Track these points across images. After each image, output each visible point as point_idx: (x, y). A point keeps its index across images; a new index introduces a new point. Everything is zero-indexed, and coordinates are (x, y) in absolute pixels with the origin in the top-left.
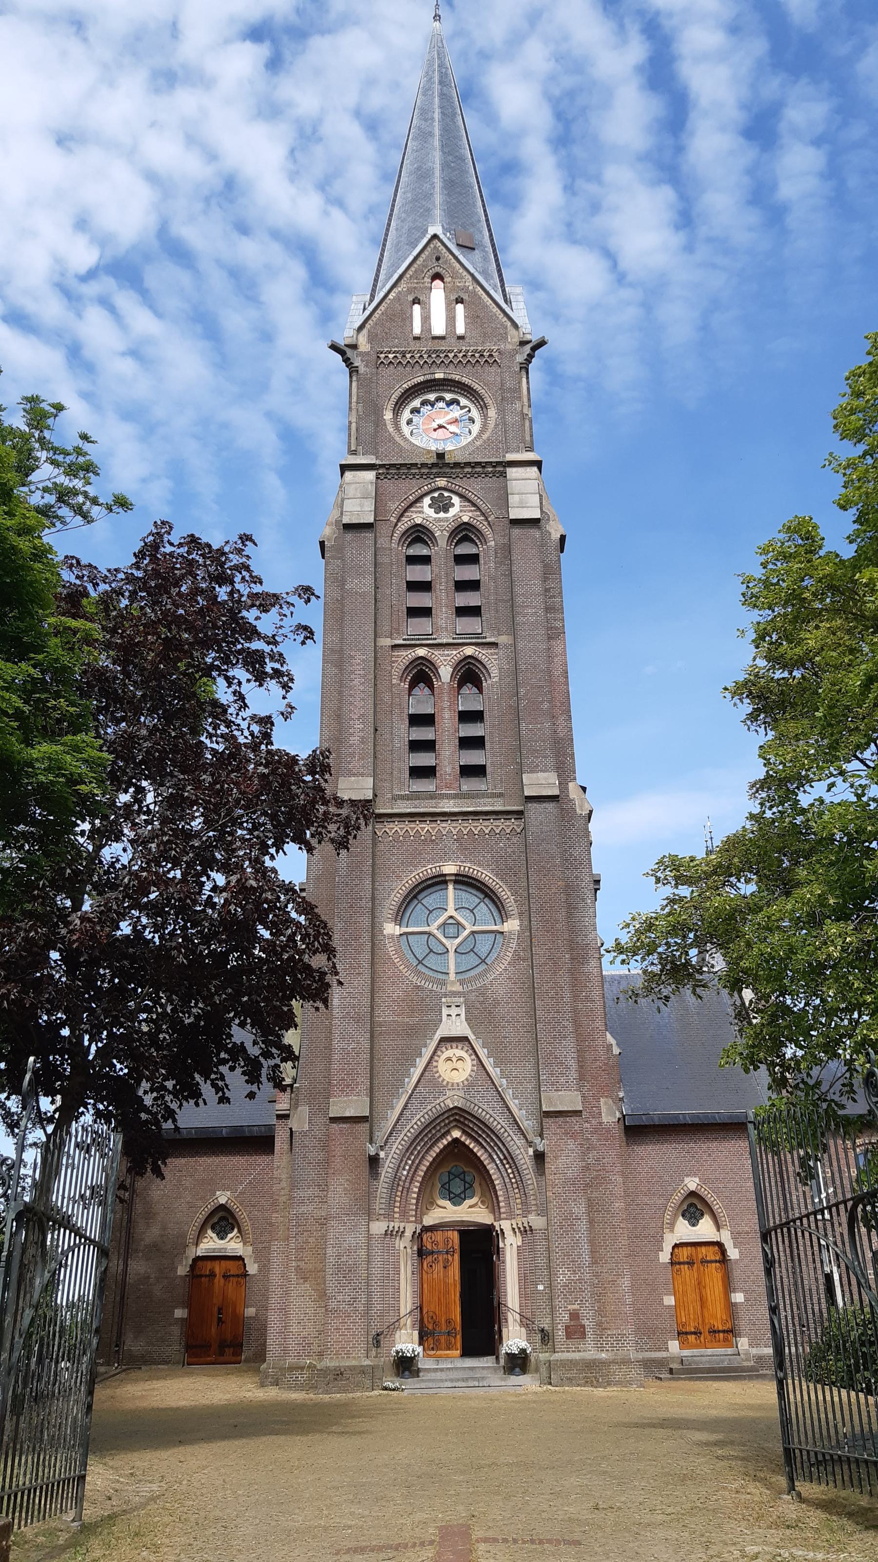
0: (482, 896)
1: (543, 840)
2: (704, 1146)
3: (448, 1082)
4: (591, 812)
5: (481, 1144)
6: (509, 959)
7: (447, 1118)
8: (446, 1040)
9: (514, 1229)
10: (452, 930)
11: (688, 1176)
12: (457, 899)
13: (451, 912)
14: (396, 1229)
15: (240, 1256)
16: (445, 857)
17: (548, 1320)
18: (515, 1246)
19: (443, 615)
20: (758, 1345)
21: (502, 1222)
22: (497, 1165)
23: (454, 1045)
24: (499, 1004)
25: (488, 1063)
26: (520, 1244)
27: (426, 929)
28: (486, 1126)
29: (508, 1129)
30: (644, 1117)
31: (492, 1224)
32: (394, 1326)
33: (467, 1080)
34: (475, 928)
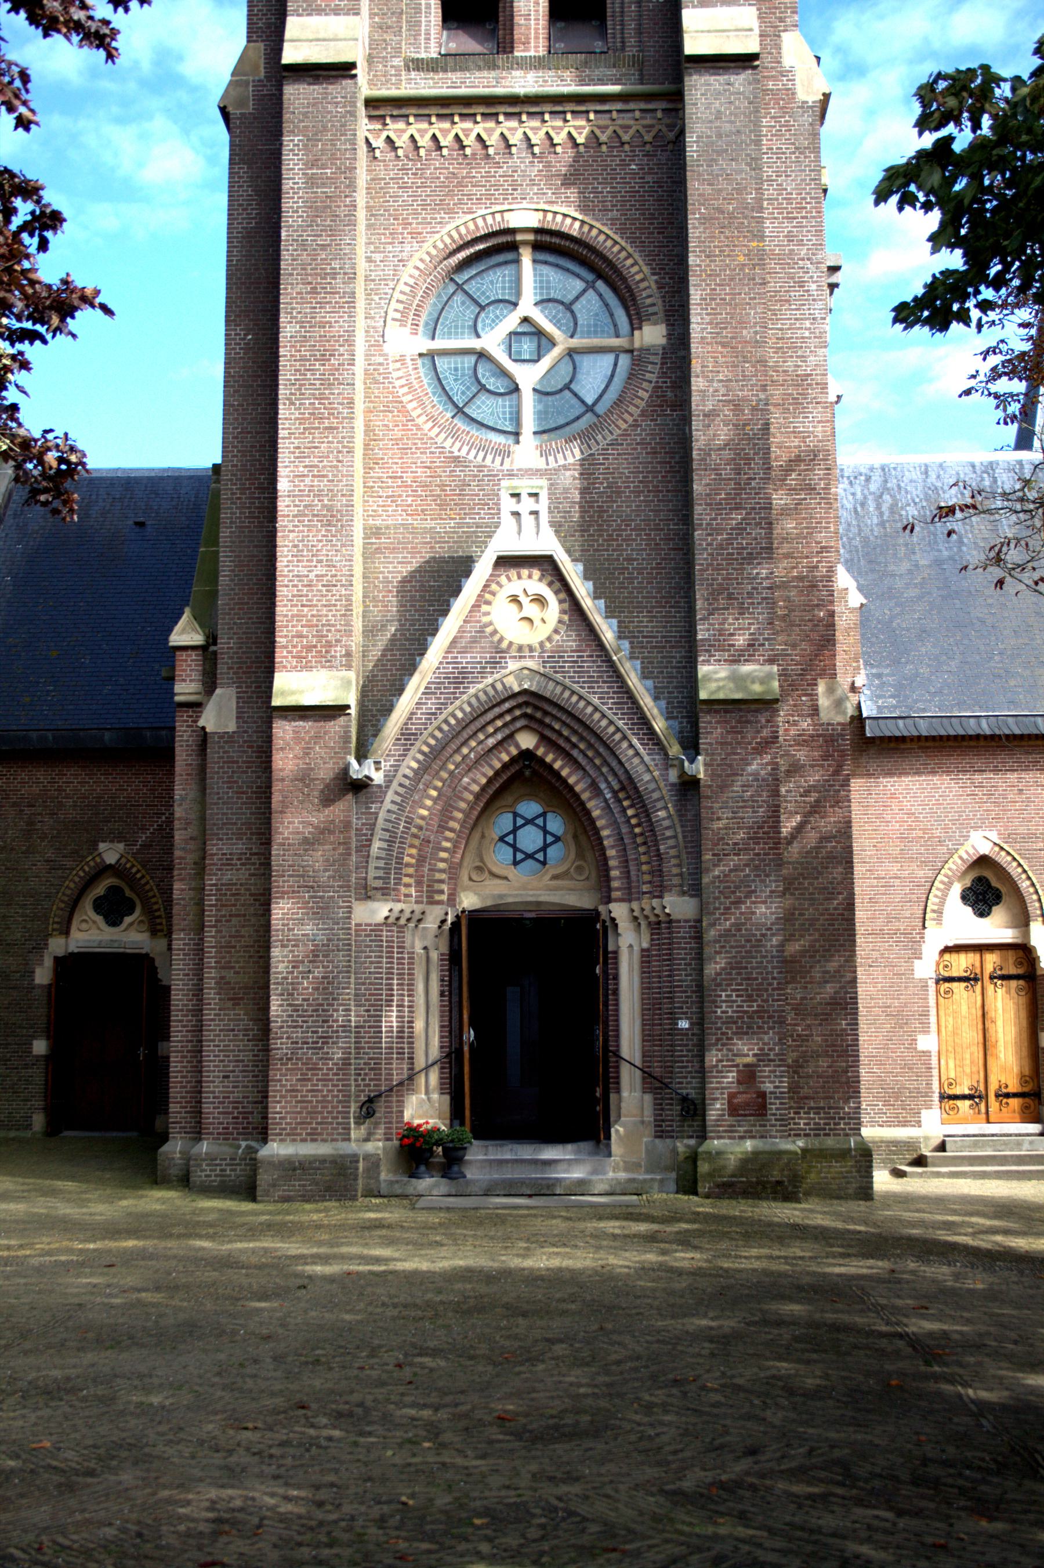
0: (590, 277)
1: (719, 153)
2: (1013, 777)
3: (511, 643)
4: (827, 97)
5: (575, 761)
6: (642, 404)
7: (509, 711)
8: (505, 562)
9: (636, 918)
10: (527, 346)
11: (976, 828)
12: (542, 285)
13: (527, 306)
14: (407, 915)
15: (147, 955)
16: (514, 189)
18: (636, 948)
19: (395, 1062)
21: (613, 906)
22: (606, 801)
23: (525, 572)
24: (619, 493)
26: (645, 945)
27: (470, 342)
28: (587, 727)
30: (901, 722)
31: (596, 910)
32: (408, 1083)
34: (575, 342)
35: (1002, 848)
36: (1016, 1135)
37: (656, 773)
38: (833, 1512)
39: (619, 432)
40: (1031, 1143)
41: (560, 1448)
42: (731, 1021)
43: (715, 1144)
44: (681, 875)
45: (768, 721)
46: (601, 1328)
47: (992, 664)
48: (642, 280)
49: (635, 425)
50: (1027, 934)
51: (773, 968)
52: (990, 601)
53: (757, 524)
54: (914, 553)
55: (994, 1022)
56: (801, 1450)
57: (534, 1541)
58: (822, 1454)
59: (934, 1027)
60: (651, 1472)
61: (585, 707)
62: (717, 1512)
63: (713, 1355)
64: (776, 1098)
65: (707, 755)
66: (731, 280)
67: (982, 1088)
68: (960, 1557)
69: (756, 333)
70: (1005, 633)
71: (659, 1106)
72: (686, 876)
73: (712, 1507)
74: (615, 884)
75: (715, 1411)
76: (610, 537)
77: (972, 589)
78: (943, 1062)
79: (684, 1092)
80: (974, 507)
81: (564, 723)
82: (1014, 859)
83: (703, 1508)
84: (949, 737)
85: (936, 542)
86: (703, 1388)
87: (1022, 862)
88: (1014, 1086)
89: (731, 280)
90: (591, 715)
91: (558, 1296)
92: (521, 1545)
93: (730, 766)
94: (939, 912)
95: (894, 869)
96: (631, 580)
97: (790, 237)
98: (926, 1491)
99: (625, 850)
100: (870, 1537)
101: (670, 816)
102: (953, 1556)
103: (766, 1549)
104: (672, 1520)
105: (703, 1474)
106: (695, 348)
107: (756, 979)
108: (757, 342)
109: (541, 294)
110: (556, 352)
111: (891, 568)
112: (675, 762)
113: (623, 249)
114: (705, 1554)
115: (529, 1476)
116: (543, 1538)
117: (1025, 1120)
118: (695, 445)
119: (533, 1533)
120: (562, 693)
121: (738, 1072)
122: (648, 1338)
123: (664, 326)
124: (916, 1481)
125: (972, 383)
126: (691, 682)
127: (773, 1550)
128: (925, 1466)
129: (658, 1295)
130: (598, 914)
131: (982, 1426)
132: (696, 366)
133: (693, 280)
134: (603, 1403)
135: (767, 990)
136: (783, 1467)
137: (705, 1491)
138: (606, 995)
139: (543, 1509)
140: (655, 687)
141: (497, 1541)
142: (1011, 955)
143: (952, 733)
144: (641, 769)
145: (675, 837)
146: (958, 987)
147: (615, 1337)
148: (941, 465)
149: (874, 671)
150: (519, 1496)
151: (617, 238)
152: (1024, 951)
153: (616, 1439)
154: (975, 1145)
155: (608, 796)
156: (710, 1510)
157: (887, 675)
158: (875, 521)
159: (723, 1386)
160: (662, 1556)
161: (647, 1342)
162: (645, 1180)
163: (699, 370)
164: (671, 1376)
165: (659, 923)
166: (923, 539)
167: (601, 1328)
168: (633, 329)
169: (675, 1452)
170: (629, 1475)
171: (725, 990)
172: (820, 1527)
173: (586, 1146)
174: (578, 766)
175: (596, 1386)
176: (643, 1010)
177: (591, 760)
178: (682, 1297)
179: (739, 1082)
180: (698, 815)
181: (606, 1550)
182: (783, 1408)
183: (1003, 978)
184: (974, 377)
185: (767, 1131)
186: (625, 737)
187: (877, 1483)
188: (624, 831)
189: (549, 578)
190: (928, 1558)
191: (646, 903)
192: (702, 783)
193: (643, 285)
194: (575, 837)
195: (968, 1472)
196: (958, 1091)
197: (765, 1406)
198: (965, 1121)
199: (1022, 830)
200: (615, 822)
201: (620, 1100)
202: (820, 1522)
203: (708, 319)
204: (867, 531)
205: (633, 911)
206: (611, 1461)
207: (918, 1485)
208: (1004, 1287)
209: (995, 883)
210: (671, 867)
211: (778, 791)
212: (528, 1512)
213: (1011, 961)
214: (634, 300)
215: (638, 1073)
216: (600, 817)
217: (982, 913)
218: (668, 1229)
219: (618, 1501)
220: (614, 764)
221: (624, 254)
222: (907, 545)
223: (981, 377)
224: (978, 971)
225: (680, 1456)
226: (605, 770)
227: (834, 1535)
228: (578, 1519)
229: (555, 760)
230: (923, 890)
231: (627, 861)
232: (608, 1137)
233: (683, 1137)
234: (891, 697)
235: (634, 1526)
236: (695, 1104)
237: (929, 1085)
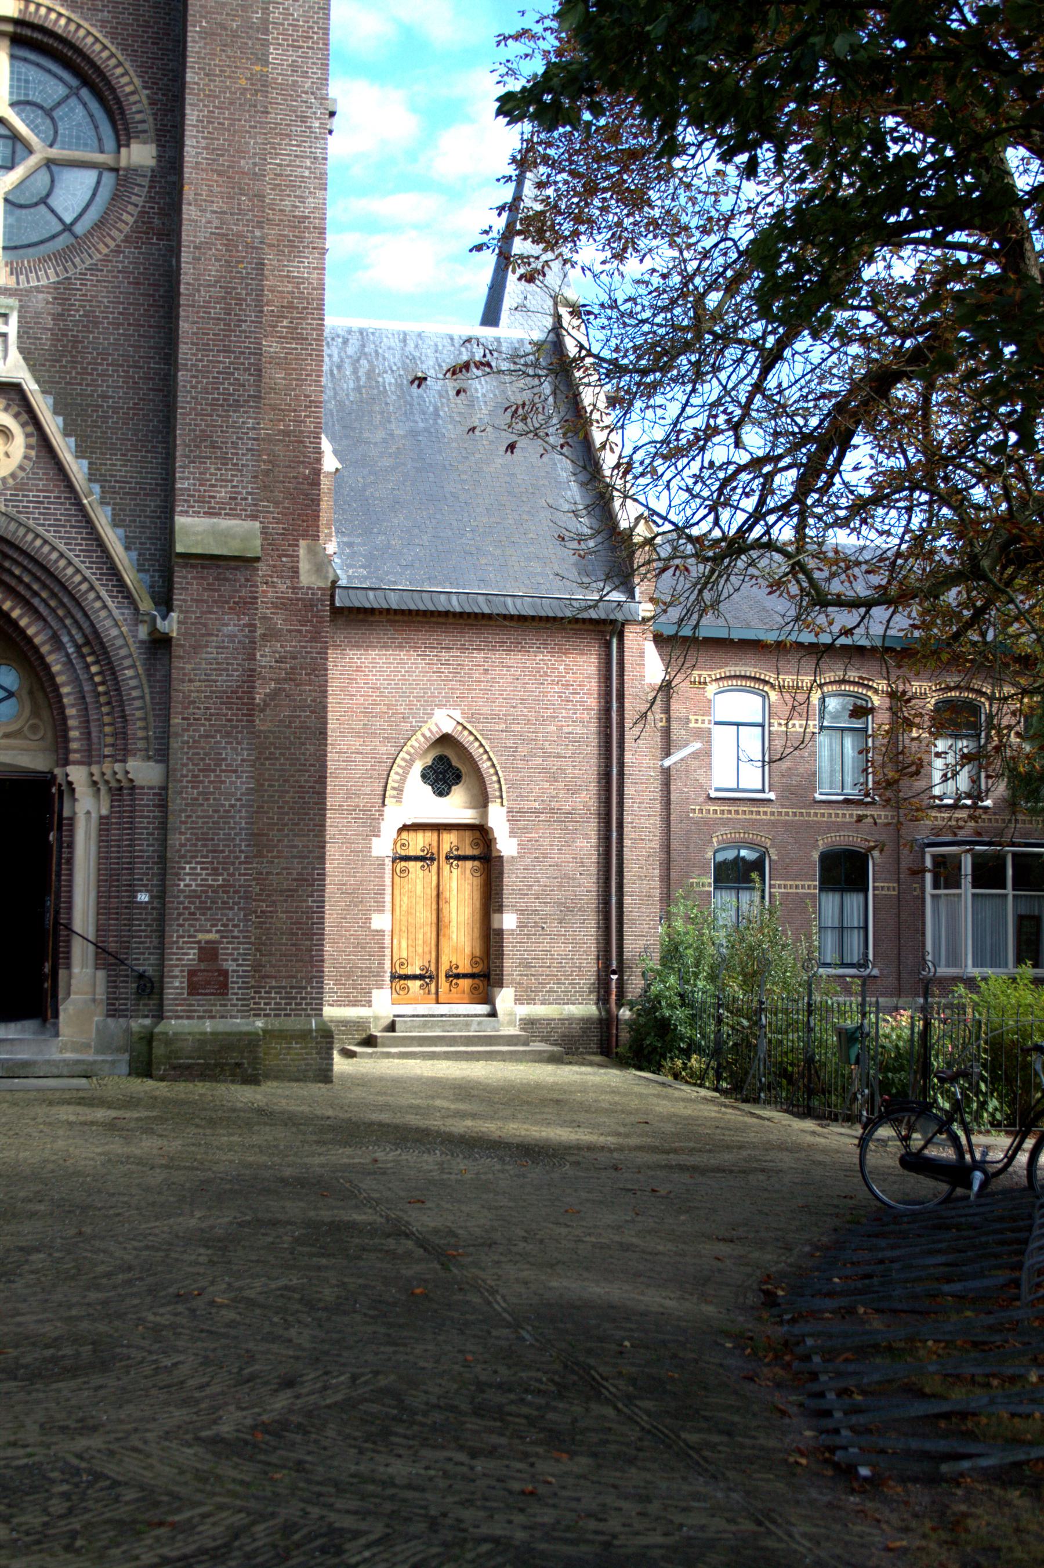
0: (74, 82)
2: (479, 656)
5: (35, 611)
6: (127, 229)
9: (95, 783)
11: (440, 706)
17: (153, 959)
18: (94, 815)
20: (531, 1001)
21: (70, 769)
22: (68, 655)
24: (96, 324)
25: (64, 447)
26: (104, 812)
28: (51, 575)
29: (97, 584)
30: (371, 594)
31: (51, 772)
33: (13, 475)
34: (54, 152)
35: (465, 728)
36: (465, 1016)
37: (124, 629)
38: (400, 1456)
39: (99, 256)
40: (479, 1023)
41: (65, 1387)
42: (194, 895)
43: (173, 1025)
44: (147, 738)
45: (247, 580)
46: (80, 1233)
47: (464, 541)
48: (133, 93)
49: (117, 251)
50: (485, 815)
51: (241, 840)
52: (464, 477)
53: (245, 370)
54: (390, 422)
55: (447, 902)
56: (342, 1378)
57: (61, 1517)
58: (366, 1383)
59: (388, 905)
60: (180, 1415)
61: (50, 552)
62: (269, 1464)
63: (212, 1263)
64: (239, 977)
65: (181, 612)
66: (231, 104)
67: (433, 968)
68: (554, 1506)
69: (255, 164)
70: (478, 510)
71: (112, 983)
72: (152, 740)
73: (262, 1457)
74: (74, 745)
75: (233, 1332)
76: (84, 372)
77: (447, 463)
79: (141, 969)
80: (489, 365)
81: (25, 568)
82: (476, 739)
83: (251, 1459)
84: (418, 612)
85: (412, 413)
86: (212, 1303)
87: (484, 742)
88: (465, 967)
89: (231, 104)
90: (56, 561)
91: (22, 1194)
92: (45, 1524)
93: (205, 625)
94: (400, 790)
95: (356, 743)
96: (105, 418)
97: (294, 66)
98: (492, 1423)
99: (86, 709)
100: (450, 1486)
101: (137, 676)
102: (547, 1505)
103: (339, 1511)
104: (219, 1478)
105: (240, 1414)
106: (188, 173)
107: (223, 851)
108: (255, 174)
109: (19, 94)
110: (33, 161)
111: (366, 435)
112: (146, 618)
113: (113, 55)
114: (271, 1523)
115: (36, 1427)
116: (70, 1512)
117: (472, 1002)
118: (184, 278)
119: (57, 1506)
120: (25, 535)
121: (200, 948)
122: (136, 1244)
123: (154, 146)
124: (479, 1411)
125: (485, 239)
126: (167, 531)
127: (348, 1512)
128: (483, 1392)
129: (133, 1191)
130: (54, 777)
131: (524, 1339)
132: (189, 193)
133: (189, 99)
134: (102, 1327)
135: (233, 863)
136: (328, 1401)
137: (248, 1437)
138: (59, 864)
139: (63, 1473)
140: (127, 537)
141: (15, 1521)
142: (468, 835)
143: (422, 608)
144: (108, 623)
145: (142, 697)
147: (97, 1243)
148: (419, 335)
149: (345, 539)
150: (30, 1455)
151: (106, 42)
152: (481, 833)
153: (128, 1373)
154: (425, 1026)
155: (71, 650)
156: (260, 1462)
157: (359, 544)
158: (352, 385)
159: (234, 1300)
160: (218, 1530)
161: (135, 1249)
162: (95, 1062)
163: (191, 197)
164: (171, 1290)
165: (121, 789)
166: (400, 408)
167: (80, 1233)
168: (119, 146)
169: (201, 1387)
170: (154, 1419)
171: (189, 863)
172: (392, 1477)
173: (30, 1025)
174: (40, 617)
175: (89, 1304)
176: (99, 881)
177: (53, 610)
178: (159, 1193)
179: (200, 960)
180: (168, 677)
181: (151, 1525)
182: (307, 1326)
183: (459, 858)
184: (486, 232)
185: (228, 1011)
186: (92, 588)
187: (437, 1417)
188: (86, 688)
189: (16, 409)
190: (522, 1510)
191: (107, 767)
192: (174, 642)
193: (134, 98)
194: (31, 693)
195: (529, 1397)
196: (409, 971)
197: (287, 1325)
198: (415, 1001)
199: (485, 710)
200: (77, 678)
201: (70, 976)
202: (390, 1470)
203: (204, 143)
204: (342, 395)
205: (92, 775)
206: (129, 1401)
207: (482, 1417)
208: (490, 1176)
209: (455, 762)
210: (136, 730)
211: (255, 655)
212: (45, 1477)
213: (468, 841)
214: (123, 113)
215: (91, 947)
216: (60, 673)
217: (442, 792)
218: (128, 1115)
219: (149, 1456)
220: (79, 616)
221: (113, 62)
222: (382, 413)
223: (494, 234)
224: (435, 851)
225: (208, 1391)
226: (68, 622)
227: (410, 1487)
228: (108, 1483)
229: (13, 608)
230: (384, 767)
231: (88, 721)
232: (56, 1015)
233: (137, 1017)
234: (361, 567)
235: (176, 1489)
236: (152, 982)
237: (381, 964)
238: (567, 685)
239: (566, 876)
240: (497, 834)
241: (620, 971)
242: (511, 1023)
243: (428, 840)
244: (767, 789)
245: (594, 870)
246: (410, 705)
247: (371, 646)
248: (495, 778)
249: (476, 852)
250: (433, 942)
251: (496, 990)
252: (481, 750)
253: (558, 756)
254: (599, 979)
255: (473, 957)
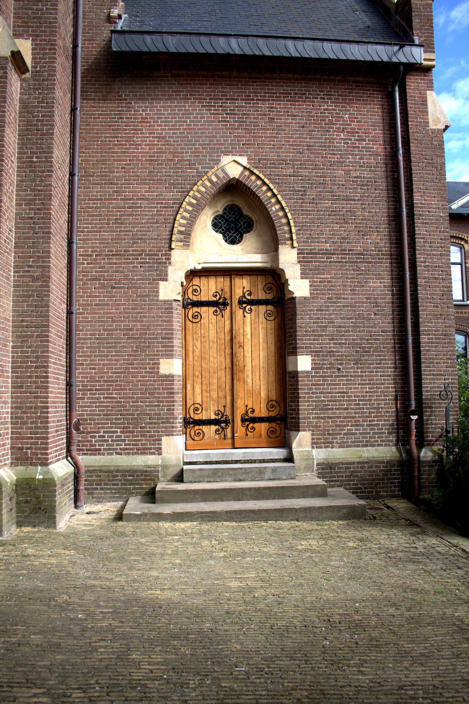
2: (264, 106)
11: (226, 153)
20: (328, 444)
35: (252, 173)
78: (189, 387)
82: (264, 183)
142: (260, 281)
146: (207, 312)
183: (252, 303)
196: (204, 416)
199: (272, 156)
209: (246, 211)
213: (260, 286)
230: (171, 212)
237: (171, 410)
238: (353, 132)
239: (360, 316)
240: (288, 275)
241: (419, 411)
242: (308, 468)
243: (220, 286)
244: (465, 300)
245: (388, 310)
246: (196, 151)
247: (156, 98)
248: (284, 221)
249: (269, 297)
250: (228, 387)
251: (293, 433)
252: (269, 194)
253: (348, 199)
254: (397, 420)
255: (269, 401)
